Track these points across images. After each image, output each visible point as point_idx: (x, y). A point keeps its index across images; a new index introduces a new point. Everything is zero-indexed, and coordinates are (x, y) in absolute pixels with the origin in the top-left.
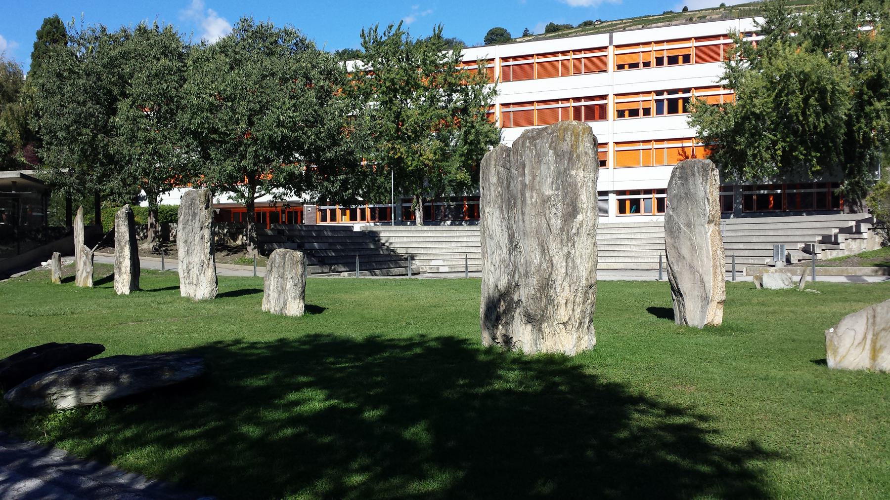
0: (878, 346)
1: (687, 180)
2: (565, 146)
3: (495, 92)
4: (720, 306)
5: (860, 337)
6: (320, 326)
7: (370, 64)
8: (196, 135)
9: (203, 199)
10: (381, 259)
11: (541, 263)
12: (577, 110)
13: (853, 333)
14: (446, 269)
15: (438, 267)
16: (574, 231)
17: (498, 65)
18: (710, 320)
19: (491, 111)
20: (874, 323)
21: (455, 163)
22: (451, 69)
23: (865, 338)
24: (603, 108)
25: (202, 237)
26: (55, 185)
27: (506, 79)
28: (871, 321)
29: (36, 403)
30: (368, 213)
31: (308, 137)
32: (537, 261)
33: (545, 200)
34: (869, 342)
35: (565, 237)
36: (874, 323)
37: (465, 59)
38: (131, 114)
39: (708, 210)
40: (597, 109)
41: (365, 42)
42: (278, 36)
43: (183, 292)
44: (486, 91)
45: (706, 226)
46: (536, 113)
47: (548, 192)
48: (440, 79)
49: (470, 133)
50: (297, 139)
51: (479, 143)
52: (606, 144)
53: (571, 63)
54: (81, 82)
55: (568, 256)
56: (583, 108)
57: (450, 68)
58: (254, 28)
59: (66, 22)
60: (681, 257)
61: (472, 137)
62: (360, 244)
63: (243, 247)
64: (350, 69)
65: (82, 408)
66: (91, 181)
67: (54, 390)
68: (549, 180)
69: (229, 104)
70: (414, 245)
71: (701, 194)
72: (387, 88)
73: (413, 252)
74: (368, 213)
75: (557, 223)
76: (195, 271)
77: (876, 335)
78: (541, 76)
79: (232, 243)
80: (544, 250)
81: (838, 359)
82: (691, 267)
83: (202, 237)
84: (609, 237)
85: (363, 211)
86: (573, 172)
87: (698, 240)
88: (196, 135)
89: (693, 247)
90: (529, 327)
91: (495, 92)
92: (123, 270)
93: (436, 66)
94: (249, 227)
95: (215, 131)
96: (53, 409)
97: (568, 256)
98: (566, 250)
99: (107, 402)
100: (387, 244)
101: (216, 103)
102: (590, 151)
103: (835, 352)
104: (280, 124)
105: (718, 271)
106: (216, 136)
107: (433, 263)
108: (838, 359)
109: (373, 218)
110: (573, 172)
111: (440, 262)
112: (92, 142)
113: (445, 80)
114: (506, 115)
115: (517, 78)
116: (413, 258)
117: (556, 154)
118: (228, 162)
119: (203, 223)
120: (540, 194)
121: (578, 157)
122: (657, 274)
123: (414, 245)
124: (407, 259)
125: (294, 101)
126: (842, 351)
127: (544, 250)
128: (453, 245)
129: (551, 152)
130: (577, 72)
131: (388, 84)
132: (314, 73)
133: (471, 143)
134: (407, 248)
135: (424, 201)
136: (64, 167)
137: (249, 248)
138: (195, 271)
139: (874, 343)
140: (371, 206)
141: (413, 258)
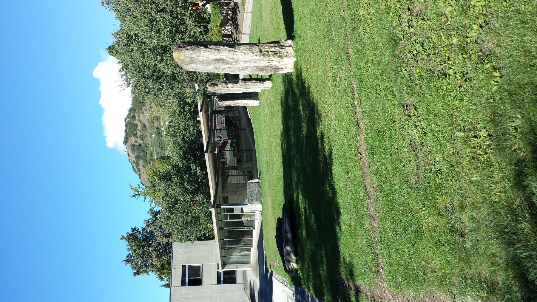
11: (248, 71)
16: (232, 60)
55: (245, 62)
59: (110, 44)
68: (206, 67)
75: (227, 66)
95: (171, 31)
96: (296, 270)
97: (245, 62)
99: (295, 256)
102: (190, 53)
117: (191, 63)
136: (195, 90)
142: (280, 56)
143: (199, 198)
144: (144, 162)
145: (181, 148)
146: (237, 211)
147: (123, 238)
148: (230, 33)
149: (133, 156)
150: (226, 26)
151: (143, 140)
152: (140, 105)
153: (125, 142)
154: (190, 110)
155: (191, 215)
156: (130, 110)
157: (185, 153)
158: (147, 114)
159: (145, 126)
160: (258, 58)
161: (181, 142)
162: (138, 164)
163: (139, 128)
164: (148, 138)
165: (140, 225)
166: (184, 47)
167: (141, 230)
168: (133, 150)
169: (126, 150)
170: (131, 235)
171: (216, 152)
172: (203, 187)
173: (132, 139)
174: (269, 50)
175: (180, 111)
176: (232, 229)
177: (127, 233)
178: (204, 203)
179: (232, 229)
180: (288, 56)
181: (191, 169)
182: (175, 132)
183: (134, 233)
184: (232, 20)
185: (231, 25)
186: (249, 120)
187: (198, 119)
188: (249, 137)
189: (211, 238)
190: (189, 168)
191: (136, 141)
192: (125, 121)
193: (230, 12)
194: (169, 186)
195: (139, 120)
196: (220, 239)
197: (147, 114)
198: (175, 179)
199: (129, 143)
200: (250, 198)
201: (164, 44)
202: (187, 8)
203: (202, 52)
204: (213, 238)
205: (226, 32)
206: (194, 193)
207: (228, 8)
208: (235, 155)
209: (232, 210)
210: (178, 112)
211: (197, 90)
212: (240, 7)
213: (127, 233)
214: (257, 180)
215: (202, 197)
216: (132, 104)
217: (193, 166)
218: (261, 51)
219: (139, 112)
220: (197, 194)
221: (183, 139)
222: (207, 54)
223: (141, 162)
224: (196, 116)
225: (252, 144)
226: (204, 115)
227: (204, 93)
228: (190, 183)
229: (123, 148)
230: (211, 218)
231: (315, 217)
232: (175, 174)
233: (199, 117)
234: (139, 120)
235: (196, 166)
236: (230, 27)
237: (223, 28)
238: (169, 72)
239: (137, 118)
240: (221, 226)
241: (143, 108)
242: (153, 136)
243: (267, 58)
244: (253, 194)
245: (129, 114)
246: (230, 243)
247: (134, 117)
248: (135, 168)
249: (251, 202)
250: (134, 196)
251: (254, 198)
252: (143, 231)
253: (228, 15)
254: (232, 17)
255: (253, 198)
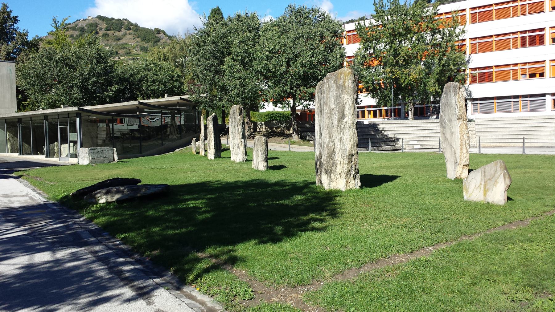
0: (487, 188)
1: (447, 95)
2: (341, 82)
3: (463, 32)
4: (465, 167)
5: (478, 184)
6: (275, 177)
7: (380, 21)
8: (261, 73)
9: (238, 110)
10: (376, 141)
11: (329, 143)
12: (523, 39)
13: (475, 181)
14: (419, 147)
15: (413, 145)
16: (343, 126)
17: (468, 13)
18: (458, 176)
19: (464, 43)
20: (485, 176)
21: (432, 80)
22: (431, 20)
23: (481, 184)
24: (542, 37)
25: (238, 130)
26: (198, 103)
27: (474, 21)
28: (483, 174)
29: (94, 200)
30: (384, 113)
31: (321, 72)
32: (327, 142)
33: (331, 111)
34: (482, 186)
35: (339, 129)
36: (485, 176)
37: (439, 12)
38: (230, 64)
39: (457, 112)
40: (537, 38)
41: (376, 8)
42: (309, 13)
43: (232, 159)
44: (457, 31)
45: (457, 121)
46: (494, 43)
47: (333, 106)
48: (424, 25)
49: (442, 59)
50: (314, 73)
51: (449, 65)
52: (544, 61)
53: (519, 8)
54: (207, 47)
55: (341, 139)
56: (527, 38)
57: (431, 19)
58: (296, 10)
59: (223, 11)
60: (446, 139)
61: (443, 62)
62: (364, 132)
63: (290, 135)
64: (367, 25)
65: (107, 203)
66: (216, 100)
67: (99, 195)
68: (333, 100)
69: (277, 55)
70: (401, 132)
71: (453, 103)
72: (389, 33)
73: (398, 136)
74: (384, 113)
75: (335, 122)
76: (236, 147)
77: (486, 182)
78: (498, 18)
79: (287, 132)
80: (331, 137)
81: (468, 195)
82: (450, 145)
83: (238, 130)
84: (536, 125)
85: (381, 111)
86: (343, 96)
87: (453, 130)
88: (261, 73)
89: (452, 134)
90: (326, 175)
91: (463, 32)
92: (211, 147)
93: (422, 18)
94: (293, 123)
95: (270, 71)
96: (97, 203)
97: (341, 139)
98: (340, 136)
99: (117, 201)
100: (383, 132)
101: (270, 55)
102: (351, 84)
103: (467, 191)
104: (304, 66)
105: (464, 147)
106: (270, 74)
107: (411, 143)
108: (468, 195)
109: (387, 116)
110: (343, 96)
111: (416, 143)
112: (213, 79)
113: (427, 26)
114: (474, 45)
115: (481, 20)
116: (398, 140)
117: (336, 86)
118: (277, 88)
119: (238, 123)
120: (329, 107)
121: (345, 87)
122: (521, 149)
123: (401, 132)
124: (394, 141)
125: (312, 51)
126: (470, 191)
127: (331, 137)
128: (427, 131)
129: (334, 85)
130: (523, 14)
131: (390, 31)
132: (327, 33)
133: (443, 66)
134: (395, 134)
135: (414, 104)
136: (202, 93)
137: (293, 135)
138: (236, 147)
139: (485, 186)
140: (386, 108)
141: (398, 140)
142: (347, 174)
143: (77, 93)
144: (77, 36)
145: (132, 75)
146: (71, 136)
147: (5, 5)
148: (258, 130)
149: (84, 25)
150: (266, 126)
151: (103, 36)
152: (143, 36)
153: (100, 17)
154: (175, 87)
155: (55, 84)
156: (136, 25)
157: (126, 80)
158: (132, 43)
159: (119, 39)
160: (347, 153)
161: (139, 76)
162: (74, 29)
163: (117, 33)
164: (106, 42)
165: (21, 27)
166: (355, 79)
167: (16, 26)
168: (91, 25)
169: (90, 18)
170: (9, 15)
171: (138, 113)
172: (92, 99)
173: (104, 26)
174: (353, 163)
175: (173, 77)
176: (46, 129)
177: (11, 11)
178: (70, 99)
179: (46, 129)
180: (347, 183)
181: (111, 85)
182: (150, 70)
183: (11, 19)
184: (272, 132)
185: (267, 130)
186: (173, 150)
187: (166, 95)
188: (148, 152)
189: (20, 107)
190: (111, 84)
191: (101, 29)
192: (124, 19)
193: (279, 130)
194: (91, 61)
195: (125, 34)
196: (19, 119)
197: (132, 43)
198: (99, 68)
199: (98, 21)
200: (96, 151)
201: (255, 63)
202: (291, 88)
203: (352, 97)
204: (19, 109)
205: (259, 126)
206: (83, 89)
207: (284, 128)
208: (123, 134)
209: (74, 130)
210: (173, 74)
211: (202, 95)
212: (287, 140)
213: (11, 11)
214: (116, 158)
215: (78, 97)
216: (143, 28)
217: (115, 88)
218: (352, 155)
219: (135, 34)
220: (81, 91)
221: (142, 78)
222: (350, 102)
223: (77, 33)
224: (168, 94)
225: (148, 152)
226: (176, 102)
227: (198, 103)
228: (94, 84)
229: (93, 13)
230: (51, 107)
231: (311, 213)
232: (105, 67)
233: (168, 96)
234: (125, 34)
235: (114, 91)
236: (264, 130)
237: (263, 123)
238: (224, 67)
239: (128, 32)
240: (49, 118)
241: (139, 39)
242: (108, 48)
243: (346, 162)
244: (101, 154)
245: (132, 24)
246: (25, 129)
247: (129, 29)
248: (70, 26)
249: (91, 153)
250: (55, 22)
251: (96, 156)
252: (13, 29)
253: (277, 128)
254: (274, 132)
255: (96, 155)
